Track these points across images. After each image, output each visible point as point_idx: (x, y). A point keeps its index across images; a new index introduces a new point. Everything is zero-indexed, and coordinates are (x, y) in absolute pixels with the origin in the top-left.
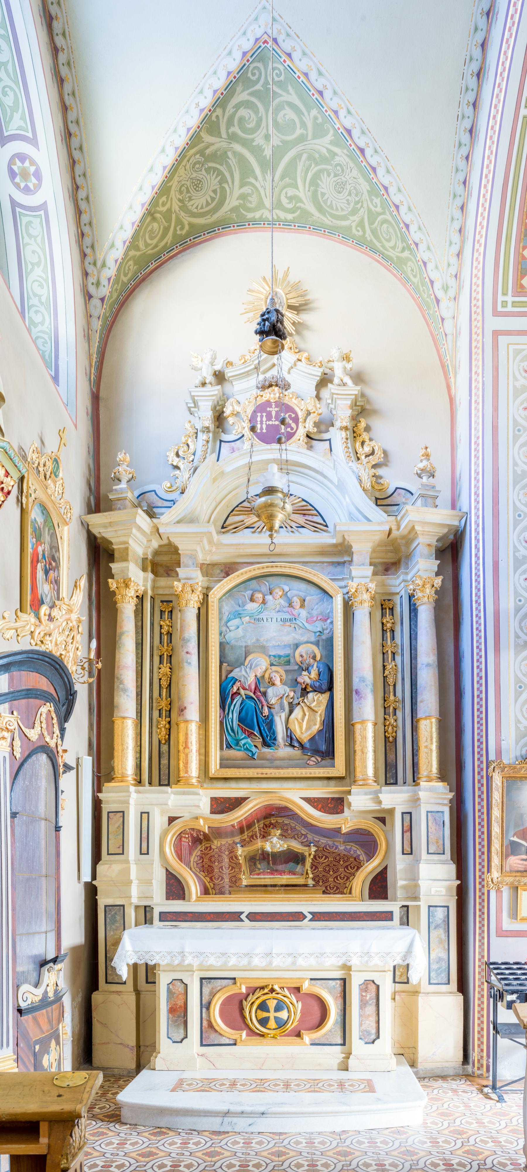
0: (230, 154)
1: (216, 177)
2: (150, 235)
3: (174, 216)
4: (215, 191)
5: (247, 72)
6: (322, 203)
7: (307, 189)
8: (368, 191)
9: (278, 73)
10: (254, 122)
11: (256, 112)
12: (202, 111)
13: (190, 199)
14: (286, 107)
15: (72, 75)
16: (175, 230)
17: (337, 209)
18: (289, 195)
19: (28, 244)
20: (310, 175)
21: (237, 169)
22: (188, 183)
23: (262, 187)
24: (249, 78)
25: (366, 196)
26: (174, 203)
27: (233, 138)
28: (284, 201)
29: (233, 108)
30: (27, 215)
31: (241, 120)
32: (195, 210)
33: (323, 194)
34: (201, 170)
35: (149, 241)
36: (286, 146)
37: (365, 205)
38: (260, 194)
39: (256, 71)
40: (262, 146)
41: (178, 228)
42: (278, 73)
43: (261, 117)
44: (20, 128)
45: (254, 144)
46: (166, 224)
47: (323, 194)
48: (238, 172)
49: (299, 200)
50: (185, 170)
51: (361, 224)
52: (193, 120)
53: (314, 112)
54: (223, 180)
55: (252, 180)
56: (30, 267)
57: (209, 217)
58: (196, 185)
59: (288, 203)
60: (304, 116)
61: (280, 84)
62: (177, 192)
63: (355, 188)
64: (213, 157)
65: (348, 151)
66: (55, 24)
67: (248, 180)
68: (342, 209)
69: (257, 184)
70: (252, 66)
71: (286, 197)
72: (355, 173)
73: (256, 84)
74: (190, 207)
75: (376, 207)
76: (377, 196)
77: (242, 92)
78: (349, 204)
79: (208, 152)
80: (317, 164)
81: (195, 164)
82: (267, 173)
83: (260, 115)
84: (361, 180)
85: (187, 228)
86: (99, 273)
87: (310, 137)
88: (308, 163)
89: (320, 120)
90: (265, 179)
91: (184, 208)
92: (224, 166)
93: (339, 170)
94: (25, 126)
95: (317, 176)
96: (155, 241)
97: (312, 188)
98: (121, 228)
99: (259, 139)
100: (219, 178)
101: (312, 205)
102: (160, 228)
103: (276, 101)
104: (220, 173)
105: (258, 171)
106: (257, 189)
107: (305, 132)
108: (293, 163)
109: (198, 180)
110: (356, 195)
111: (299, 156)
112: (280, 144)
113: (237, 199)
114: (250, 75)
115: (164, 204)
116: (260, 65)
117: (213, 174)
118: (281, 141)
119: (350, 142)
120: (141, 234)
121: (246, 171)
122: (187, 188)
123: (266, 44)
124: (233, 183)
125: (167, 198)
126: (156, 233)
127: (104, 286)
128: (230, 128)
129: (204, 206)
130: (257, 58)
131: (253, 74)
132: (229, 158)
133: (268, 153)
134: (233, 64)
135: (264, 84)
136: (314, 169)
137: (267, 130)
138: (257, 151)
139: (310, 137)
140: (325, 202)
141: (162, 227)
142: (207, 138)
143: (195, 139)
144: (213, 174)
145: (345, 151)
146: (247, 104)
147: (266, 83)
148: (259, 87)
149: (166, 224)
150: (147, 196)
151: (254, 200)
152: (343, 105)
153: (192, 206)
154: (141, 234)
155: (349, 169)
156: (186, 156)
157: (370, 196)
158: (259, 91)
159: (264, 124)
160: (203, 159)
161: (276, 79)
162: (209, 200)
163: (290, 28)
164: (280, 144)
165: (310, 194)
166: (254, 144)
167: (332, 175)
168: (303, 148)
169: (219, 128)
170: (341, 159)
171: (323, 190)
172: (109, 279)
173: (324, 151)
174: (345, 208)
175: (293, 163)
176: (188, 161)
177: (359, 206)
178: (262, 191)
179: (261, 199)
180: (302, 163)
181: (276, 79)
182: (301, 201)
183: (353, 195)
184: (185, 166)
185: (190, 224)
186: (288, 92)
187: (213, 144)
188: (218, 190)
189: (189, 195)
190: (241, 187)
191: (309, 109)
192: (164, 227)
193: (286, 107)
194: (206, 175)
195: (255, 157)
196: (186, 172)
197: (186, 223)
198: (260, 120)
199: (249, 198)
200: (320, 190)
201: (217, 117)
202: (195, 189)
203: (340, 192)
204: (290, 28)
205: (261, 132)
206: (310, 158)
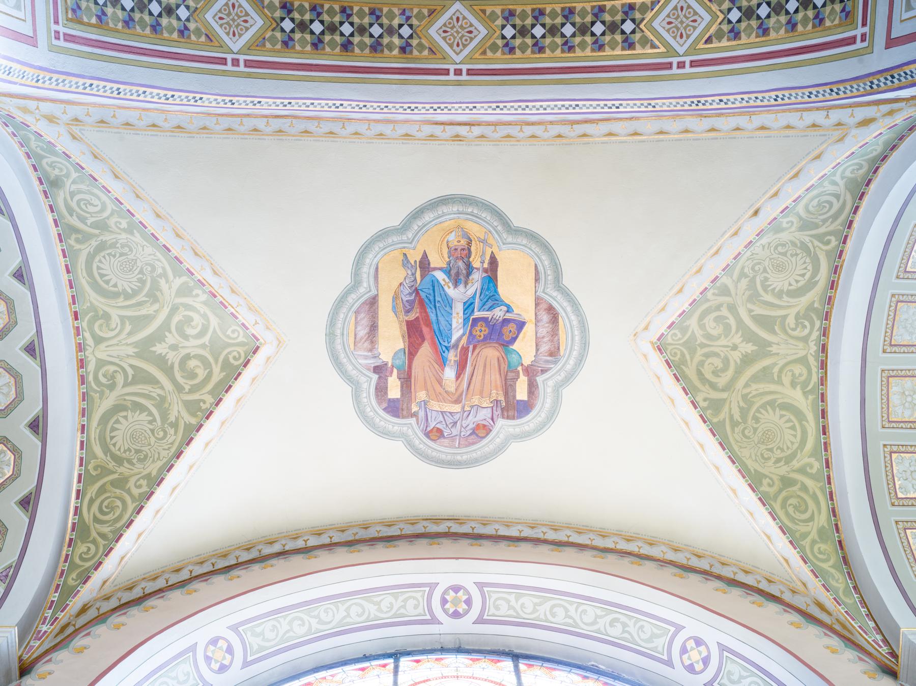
3: (97, 232)
4: (115, 286)
8: (150, 474)
35: (76, 198)
49: (112, 387)
51: (819, 238)
55: (128, 328)
57: (85, 274)
82: (135, 347)
95: (142, 408)
100: (130, 291)
102: (799, 496)
105: (766, 362)
112: (169, 363)
122: (126, 254)
129: (100, 271)
133: (749, 348)
138: (747, 360)
141: (799, 493)
149: (89, 222)
150: (749, 498)
162: (106, 278)
164: (169, 363)
175: (760, 320)
184: (741, 447)
188: (116, 289)
190: (119, 316)
192: (86, 218)
197: (82, 247)
201: (197, 295)
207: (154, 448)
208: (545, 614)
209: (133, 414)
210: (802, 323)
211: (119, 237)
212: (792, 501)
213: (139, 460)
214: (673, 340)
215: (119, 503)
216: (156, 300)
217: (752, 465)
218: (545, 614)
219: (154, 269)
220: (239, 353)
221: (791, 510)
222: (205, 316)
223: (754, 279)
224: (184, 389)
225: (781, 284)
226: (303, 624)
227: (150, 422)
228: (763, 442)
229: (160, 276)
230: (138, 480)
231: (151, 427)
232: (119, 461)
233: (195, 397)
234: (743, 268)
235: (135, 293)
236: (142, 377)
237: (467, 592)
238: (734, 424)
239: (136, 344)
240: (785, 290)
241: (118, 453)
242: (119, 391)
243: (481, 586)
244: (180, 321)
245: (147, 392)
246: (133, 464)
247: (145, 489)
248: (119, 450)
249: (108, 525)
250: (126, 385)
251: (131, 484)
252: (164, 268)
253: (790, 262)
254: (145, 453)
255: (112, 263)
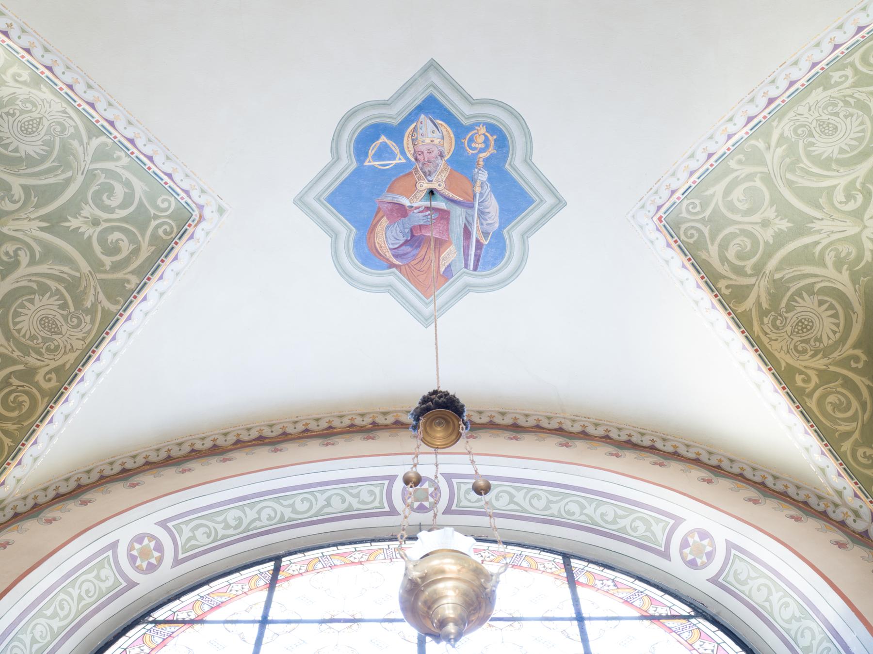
0: (777, 276)
1: (803, 298)
2: (840, 411)
3: (832, 368)
4: (16, 150)
5: (688, 243)
6: (855, 152)
7: (835, 174)
8: (825, 89)
9: (692, 206)
10: (745, 239)
11: (734, 235)
12: (713, 307)
13: (819, 340)
14: (729, 199)
15: (673, 440)
16: (855, 370)
17: (863, 131)
18: (844, 200)
19: (750, 591)
20: (815, 170)
21: (799, 268)
22: (796, 339)
23: (829, 236)
24: (695, 242)
25: (833, 92)
26: (813, 365)
27: (758, 270)
28: (852, 206)
29: (723, 265)
30: (728, 574)
31: (740, 256)
32: (838, 335)
33: (842, 151)
34: (786, 318)
35: (849, 414)
36: (777, 200)
37: (849, 92)
38: (839, 240)
39: (689, 233)
40: (775, 232)
41: (853, 365)
42: (692, 206)
43: (740, 230)
44: (664, 530)
45: (771, 242)
46: (840, 381)
47: (842, 151)
48: (802, 268)
50: (776, 340)
52: (721, 318)
53: (732, 164)
54: (809, 290)
55: (819, 248)
56: (767, 605)
57: (854, 317)
58: (802, 329)
59: (855, 200)
60: (739, 176)
61: (704, 205)
62: (801, 358)
63: (825, 108)
64: (775, 299)
65: (774, 120)
66: (634, 439)
67: (817, 254)
68: (862, 123)
69: (825, 242)
70: (683, 237)
71: (846, 203)
72: (802, 109)
73: (703, 233)
74: (830, 342)
75: (847, 77)
76: (829, 78)
77: (708, 251)
78: (851, 115)
79: (765, 305)
80: (799, 160)
81: (774, 326)
82: (812, 228)
83: (737, 231)
84: (811, 99)
85: (858, 352)
86: (845, 505)
87: (764, 169)
88: (798, 172)
89: (741, 156)
90: (819, 232)
91: (826, 352)
92: (791, 285)
93: (803, 131)
94: (664, 523)
95: (816, 160)
96: (855, 404)
97: (834, 166)
98: (807, 449)
99: (767, 235)
100: (805, 294)
101: (859, 167)
102: (839, 393)
103: (724, 211)
104: (798, 293)
105: (807, 240)
106: (831, 243)
107: (759, 175)
108: (801, 193)
109: (797, 324)
110: (836, 105)
111: (790, 184)
112: (774, 208)
113: (841, 273)
114: (691, 241)
115: (807, 380)
116: (683, 227)
117: (797, 302)
118: (771, 206)
119: (760, 118)
120: (828, 424)
121: (805, 256)
123: (663, 219)
124: (816, 276)
125: (801, 372)
126: (843, 399)
127: (861, 507)
128: (746, 272)
129: (838, 321)
130: (676, 230)
131: (692, 236)
132: (783, 278)
133: (784, 225)
134: (677, 259)
135: (704, 224)
136: (806, 163)
137: (756, 223)
138: (781, 239)
139: (765, 170)
140: (852, 148)
141: (839, 389)
142: (749, 303)
143: (742, 322)
144: (797, 302)
145: (775, 124)
146: (723, 247)
147: (702, 221)
148: (706, 231)
151: (846, 249)
152: (723, 127)
153: (829, 338)
154: (828, 424)
155: (799, 117)
156: (758, 337)
157: (832, 87)
158: (710, 230)
159: (749, 227)
160: (773, 313)
161: (698, 209)
163: (651, 189)
164: (774, 208)
165: (842, 170)
166: (771, 242)
167: (811, 139)
168: (779, 178)
169: (741, 286)
170: (786, 128)
171: (836, 152)
172: (856, 496)
173: (780, 151)
174: (860, 119)
175: (801, 193)
176: (766, 334)
177: (851, 100)
178: (834, 237)
179: (845, 239)
180: (800, 180)
181: (698, 209)
182: (853, 183)
183: (836, 110)
184: (771, 340)
185: (855, 346)
186: (713, 195)
187: (759, 296)
188: (18, 155)
189: (812, 340)
190: (824, 265)
191: (729, 171)
192: (842, 386)
193: (729, 199)
194: (795, 312)
195: (788, 242)
196: (780, 339)
198: (744, 233)
199: (842, 255)
200: (835, 155)
201: (727, 287)
202: (808, 330)
203: (836, 128)
204: (651, 189)
205: (758, 230)
206: (791, 168)
207: (65, 338)
208: (796, 634)
209: (41, 297)
210: (11, 257)
211: (18, 91)
212: (832, 398)
213: (48, 349)
214: (688, 211)
215: (25, 398)
216: (68, 166)
217: (785, 359)
218: (796, 634)
219: (64, 129)
220: (172, 227)
221: (829, 409)
222: (128, 184)
223: (76, 309)
224: (103, 265)
225: (830, 150)
226: (533, 497)
227: (813, 144)
228: (798, 333)
229: (72, 137)
230: (47, 373)
231: (65, 313)
232: (25, 350)
233: (119, 275)
234: (93, 322)
235: (43, 159)
236: (50, 253)
237: (152, 537)
238: (763, 313)
239: (42, 218)
240: (834, 158)
241: (22, 340)
242: (22, 270)
243: (163, 524)
244: (97, 191)
245: (57, 273)
246: (41, 354)
247: (54, 383)
248: (24, 336)
249: (13, 422)
250: (32, 262)
251: (39, 378)
252: (76, 128)
253: (37, 330)
254: (825, 111)
255: (11, 123)
